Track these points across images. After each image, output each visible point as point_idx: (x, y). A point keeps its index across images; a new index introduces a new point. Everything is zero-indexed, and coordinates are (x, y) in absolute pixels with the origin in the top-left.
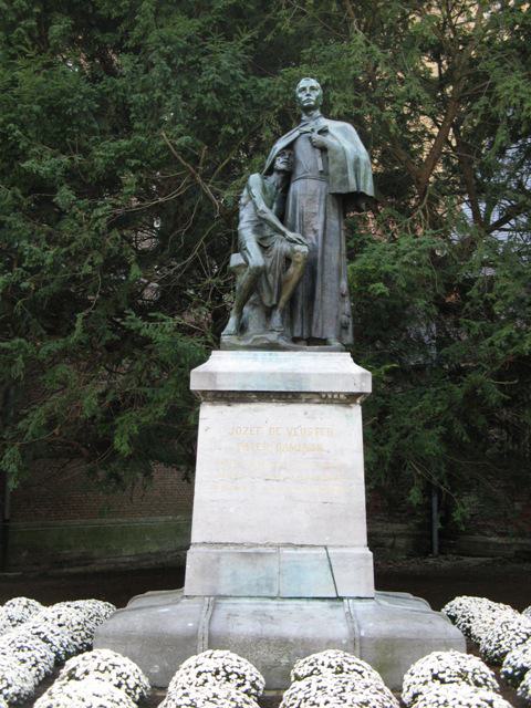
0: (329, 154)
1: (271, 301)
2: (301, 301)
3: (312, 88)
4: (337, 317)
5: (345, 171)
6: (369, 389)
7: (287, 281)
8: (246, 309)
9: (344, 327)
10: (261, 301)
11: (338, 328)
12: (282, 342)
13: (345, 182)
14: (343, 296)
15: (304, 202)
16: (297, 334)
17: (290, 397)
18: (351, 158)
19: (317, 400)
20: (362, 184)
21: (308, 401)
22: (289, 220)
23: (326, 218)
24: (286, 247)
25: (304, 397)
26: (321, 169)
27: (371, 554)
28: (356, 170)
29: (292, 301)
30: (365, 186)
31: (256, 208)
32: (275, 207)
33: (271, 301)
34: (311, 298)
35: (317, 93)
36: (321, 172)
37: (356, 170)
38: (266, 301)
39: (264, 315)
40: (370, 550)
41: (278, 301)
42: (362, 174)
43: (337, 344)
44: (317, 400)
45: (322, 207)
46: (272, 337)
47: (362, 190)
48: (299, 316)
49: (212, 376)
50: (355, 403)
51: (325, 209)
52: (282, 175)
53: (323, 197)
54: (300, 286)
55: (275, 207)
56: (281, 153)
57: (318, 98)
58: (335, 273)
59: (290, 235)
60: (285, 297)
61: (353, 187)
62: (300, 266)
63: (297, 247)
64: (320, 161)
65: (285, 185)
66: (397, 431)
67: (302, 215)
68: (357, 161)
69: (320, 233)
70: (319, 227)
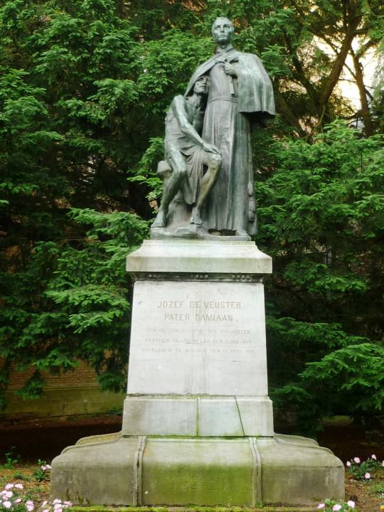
0: (239, 79)
5: (251, 94)
6: (270, 271)
13: (251, 103)
14: (250, 196)
16: (213, 226)
28: (260, 93)
32: (194, 123)
37: (260, 93)
44: (229, 280)
46: (193, 229)
52: (200, 97)
56: (201, 79)
60: (202, 196)
61: (257, 109)
63: (214, 156)
69: (231, 144)
70: (231, 140)
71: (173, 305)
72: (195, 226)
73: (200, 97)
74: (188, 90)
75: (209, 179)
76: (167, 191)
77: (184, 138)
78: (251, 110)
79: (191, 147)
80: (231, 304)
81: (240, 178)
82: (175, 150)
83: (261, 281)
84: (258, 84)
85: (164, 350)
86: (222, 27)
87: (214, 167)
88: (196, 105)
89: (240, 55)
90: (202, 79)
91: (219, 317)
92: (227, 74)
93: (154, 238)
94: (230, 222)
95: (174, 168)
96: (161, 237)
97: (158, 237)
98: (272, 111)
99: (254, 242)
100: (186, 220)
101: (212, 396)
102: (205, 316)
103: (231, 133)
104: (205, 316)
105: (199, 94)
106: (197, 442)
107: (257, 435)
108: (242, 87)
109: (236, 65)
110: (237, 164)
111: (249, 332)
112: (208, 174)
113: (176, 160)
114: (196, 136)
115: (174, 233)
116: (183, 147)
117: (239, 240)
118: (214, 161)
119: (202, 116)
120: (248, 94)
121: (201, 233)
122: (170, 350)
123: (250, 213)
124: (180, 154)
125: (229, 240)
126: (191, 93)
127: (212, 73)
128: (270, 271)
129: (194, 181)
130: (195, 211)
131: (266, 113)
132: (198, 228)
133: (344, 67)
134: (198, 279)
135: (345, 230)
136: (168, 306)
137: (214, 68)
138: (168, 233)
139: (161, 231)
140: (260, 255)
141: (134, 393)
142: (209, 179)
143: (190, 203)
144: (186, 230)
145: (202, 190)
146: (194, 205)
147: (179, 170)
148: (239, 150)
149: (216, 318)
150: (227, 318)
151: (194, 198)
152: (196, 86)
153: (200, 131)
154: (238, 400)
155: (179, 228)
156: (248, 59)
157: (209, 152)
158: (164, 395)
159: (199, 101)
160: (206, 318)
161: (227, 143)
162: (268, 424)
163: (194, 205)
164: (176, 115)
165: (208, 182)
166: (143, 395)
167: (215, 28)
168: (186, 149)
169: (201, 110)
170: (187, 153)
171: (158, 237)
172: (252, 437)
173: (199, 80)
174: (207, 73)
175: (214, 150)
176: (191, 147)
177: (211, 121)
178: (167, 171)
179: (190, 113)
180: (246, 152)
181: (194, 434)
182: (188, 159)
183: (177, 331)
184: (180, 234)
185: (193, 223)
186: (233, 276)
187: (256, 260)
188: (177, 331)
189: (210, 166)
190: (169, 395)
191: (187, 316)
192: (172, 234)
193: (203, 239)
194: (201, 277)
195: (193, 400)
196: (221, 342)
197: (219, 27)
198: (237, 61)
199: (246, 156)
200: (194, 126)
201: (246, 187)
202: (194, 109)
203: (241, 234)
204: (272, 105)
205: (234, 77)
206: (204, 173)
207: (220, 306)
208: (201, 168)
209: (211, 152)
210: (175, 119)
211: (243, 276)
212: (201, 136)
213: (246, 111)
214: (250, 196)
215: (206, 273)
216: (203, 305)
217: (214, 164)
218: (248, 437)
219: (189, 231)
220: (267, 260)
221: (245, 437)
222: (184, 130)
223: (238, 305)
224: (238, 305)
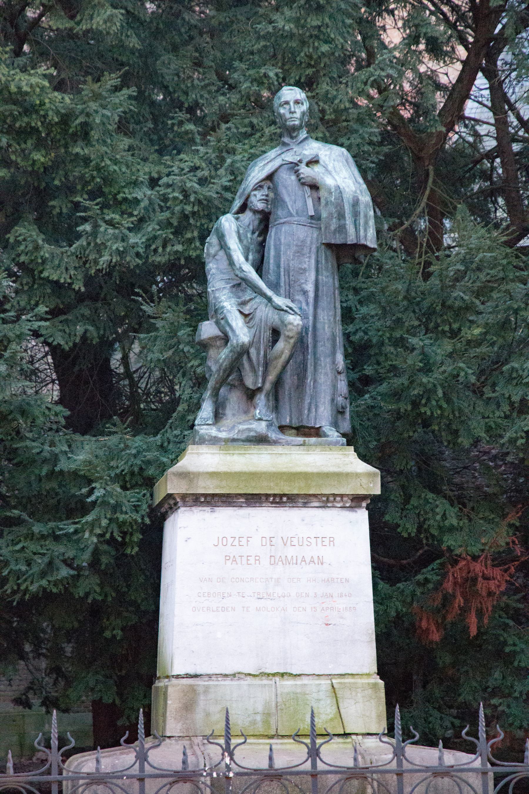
0: (323, 193)
1: (255, 383)
2: (289, 380)
3: (297, 102)
4: (333, 400)
5: (341, 216)
6: (377, 491)
7: (276, 358)
8: (223, 391)
9: (341, 412)
10: (241, 380)
11: (335, 413)
12: (273, 435)
13: (342, 229)
14: (339, 373)
15: (290, 253)
16: (287, 421)
17: (209, 499)
18: (348, 196)
19: (317, 504)
20: (362, 233)
21: (305, 505)
22: (272, 277)
23: (317, 257)
24: (274, 317)
25: (263, 498)
26: (312, 212)
27: (381, 683)
28: (356, 215)
29: (278, 384)
30: (366, 236)
31: (231, 262)
32: (251, 257)
33: (255, 383)
34: (301, 376)
35: (305, 107)
36: (312, 217)
37: (356, 215)
38: (249, 382)
39: (245, 398)
40: (381, 678)
41: (264, 382)
42: (362, 221)
43: (333, 435)
44: (317, 504)
45: (313, 261)
46: (261, 427)
47: (363, 242)
48: (287, 397)
49: (185, 475)
50: (360, 507)
51: (317, 262)
52: (258, 216)
53: (314, 249)
54: (289, 367)
55: (251, 257)
56: (259, 187)
57: (303, 114)
58: (328, 345)
59: (278, 301)
60: (272, 377)
61: (351, 239)
62: (292, 341)
63: (291, 318)
64: (310, 202)
65: (262, 227)
66: (393, 240)
67: (288, 272)
68: (356, 203)
69: (311, 295)
70: (310, 287)
71: (236, 543)
72: (264, 424)
73: (258, 216)
74: (237, 204)
75: (282, 352)
76: (218, 371)
77: (239, 285)
78: (338, 240)
79: (251, 299)
80: (321, 539)
81: (324, 348)
82: (229, 307)
83: (364, 504)
84: (351, 201)
85: (224, 609)
86: (292, 103)
87: (291, 334)
88: (251, 227)
89: (319, 149)
90: (261, 187)
91: (303, 560)
92: (303, 184)
93: (202, 441)
94: (313, 414)
95: (230, 334)
96: (214, 441)
97: (209, 441)
98: (372, 243)
99: (352, 448)
100: (246, 412)
101: (296, 675)
102: (283, 558)
103: (312, 276)
104: (283, 558)
105: (255, 212)
106: (282, 744)
107: (364, 731)
108: (327, 204)
109: (317, 169)
110: (319, 326)
111: (347, 581)
112: (280, 345)
113: (234, 324)
114: (253, 275)
115: (233, 435)
116: (240, 300)
117: (330, 444)
118: (290, 327)
119: (262, 245)
120: (335, 215)
121: (273, 435)
122: (233, 609)
123: (340, 400)
124: (238, 313)
125: (316, 445)
126: (243, 208)
127: (276, 178)
128: (377, 491)
129: (258, 354)
130: (261, 400)
131: (365, 247)
132: (268, 426)
133: (489, 104)
134: (272, 503)
135: (132, 267)
136: (237, 539)
137: (281, 170)
138: (223, 435)
139: (213, 432)
140: (363, 467)
141: (182, 672)
142: (282, 352)
143: (251, 387)
144: (249, 430)
145: (271, 368)
146: (259, 389)
147: (240, 341)
148: (324, 303)
149: (299, 561)
150: (316, 561)
151: (260, 380)
152: (252, 198)
153: (259, 268)
154: (334, 681)
155: (241, 427)
156: (333, 156)
157: (283, 310)
158: (226, 676)
159: (256, 223)
160: (286, 561)
161: (305, 293)
162: (379, 716)
163: (259, 389)
164: (223, 246)
165: (280, 356)
166: (196, 676)
167: (281, 105)
168: (244, 303)
169: (259, 235)
170: (247, 310)
171: (209, 441)
172: (357, 734)
173: (255, 189)
174: (270, 177)
175: (291, 308)
176: (251, 299)
177: (278, 256)
178: (216, 338)
179: (245, 242)
180: (332, 306)
181: (273, 733)
182: (248, 319)
183: (242, 580)
184: (243, 436)
185: (260, 419)
186: (325, 499)
187: (357, 475)
188: (242, 580)
189: (285, 332)
190: (234, 675)
191: (258, 559)
192: (231, 435)
193: (275, 443)
194: (278, 500)
195: (270, 682)
196: (307, 595)
197: (287, 103)
198: (317, 162)
199: (331, 313)
200: (250, 262)
201: (334, 362)
202: (249, 235)
203: (329, 433)
204: (372, 232)
205: (314, 187)
206: (275, 341)
207: (306, 543)
208: (268, 333)
209: (286, 311)
210: (222, 253)
211: (338, 499)
212: (261, 276)
213: (333, 242)
214: (339, 373)
215: (285, 495)
216: (280, 541)
217: (290, 330)
218: (350, 734)
219: (256, 432)
220: (375, 474)
221: (346, 735)
222: (241, 275)
223: (332, 540)
224: (332, 540)
